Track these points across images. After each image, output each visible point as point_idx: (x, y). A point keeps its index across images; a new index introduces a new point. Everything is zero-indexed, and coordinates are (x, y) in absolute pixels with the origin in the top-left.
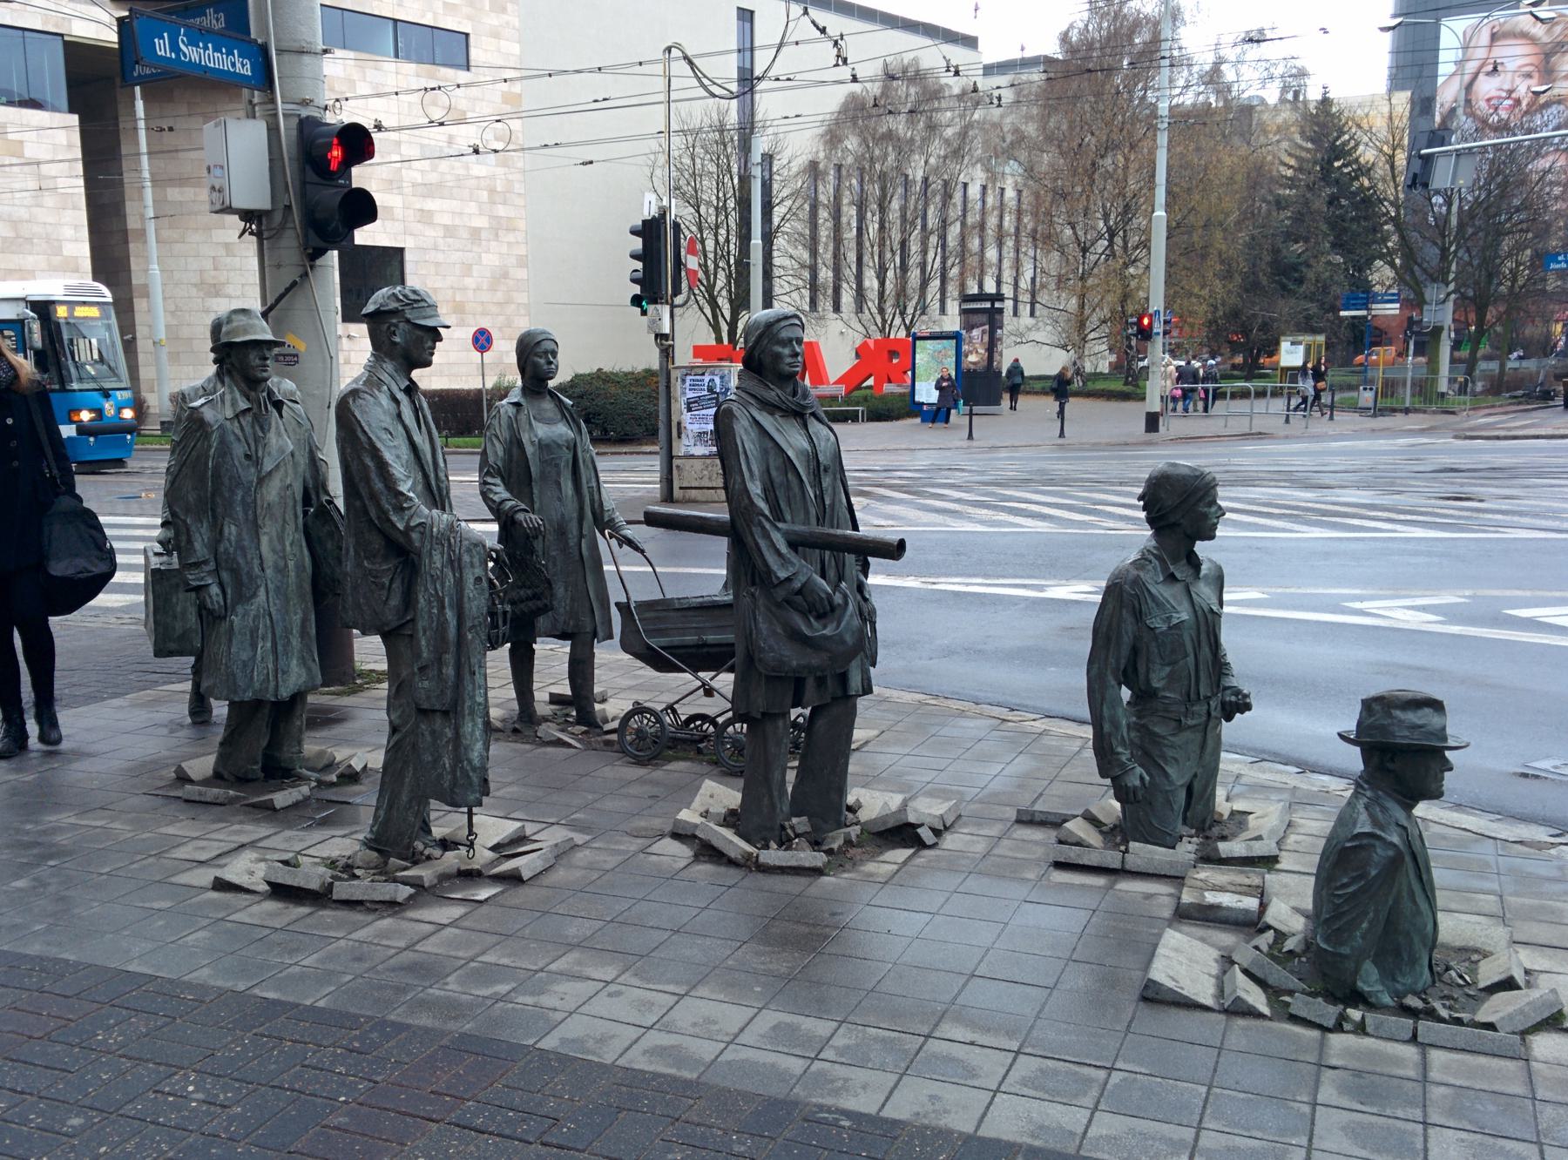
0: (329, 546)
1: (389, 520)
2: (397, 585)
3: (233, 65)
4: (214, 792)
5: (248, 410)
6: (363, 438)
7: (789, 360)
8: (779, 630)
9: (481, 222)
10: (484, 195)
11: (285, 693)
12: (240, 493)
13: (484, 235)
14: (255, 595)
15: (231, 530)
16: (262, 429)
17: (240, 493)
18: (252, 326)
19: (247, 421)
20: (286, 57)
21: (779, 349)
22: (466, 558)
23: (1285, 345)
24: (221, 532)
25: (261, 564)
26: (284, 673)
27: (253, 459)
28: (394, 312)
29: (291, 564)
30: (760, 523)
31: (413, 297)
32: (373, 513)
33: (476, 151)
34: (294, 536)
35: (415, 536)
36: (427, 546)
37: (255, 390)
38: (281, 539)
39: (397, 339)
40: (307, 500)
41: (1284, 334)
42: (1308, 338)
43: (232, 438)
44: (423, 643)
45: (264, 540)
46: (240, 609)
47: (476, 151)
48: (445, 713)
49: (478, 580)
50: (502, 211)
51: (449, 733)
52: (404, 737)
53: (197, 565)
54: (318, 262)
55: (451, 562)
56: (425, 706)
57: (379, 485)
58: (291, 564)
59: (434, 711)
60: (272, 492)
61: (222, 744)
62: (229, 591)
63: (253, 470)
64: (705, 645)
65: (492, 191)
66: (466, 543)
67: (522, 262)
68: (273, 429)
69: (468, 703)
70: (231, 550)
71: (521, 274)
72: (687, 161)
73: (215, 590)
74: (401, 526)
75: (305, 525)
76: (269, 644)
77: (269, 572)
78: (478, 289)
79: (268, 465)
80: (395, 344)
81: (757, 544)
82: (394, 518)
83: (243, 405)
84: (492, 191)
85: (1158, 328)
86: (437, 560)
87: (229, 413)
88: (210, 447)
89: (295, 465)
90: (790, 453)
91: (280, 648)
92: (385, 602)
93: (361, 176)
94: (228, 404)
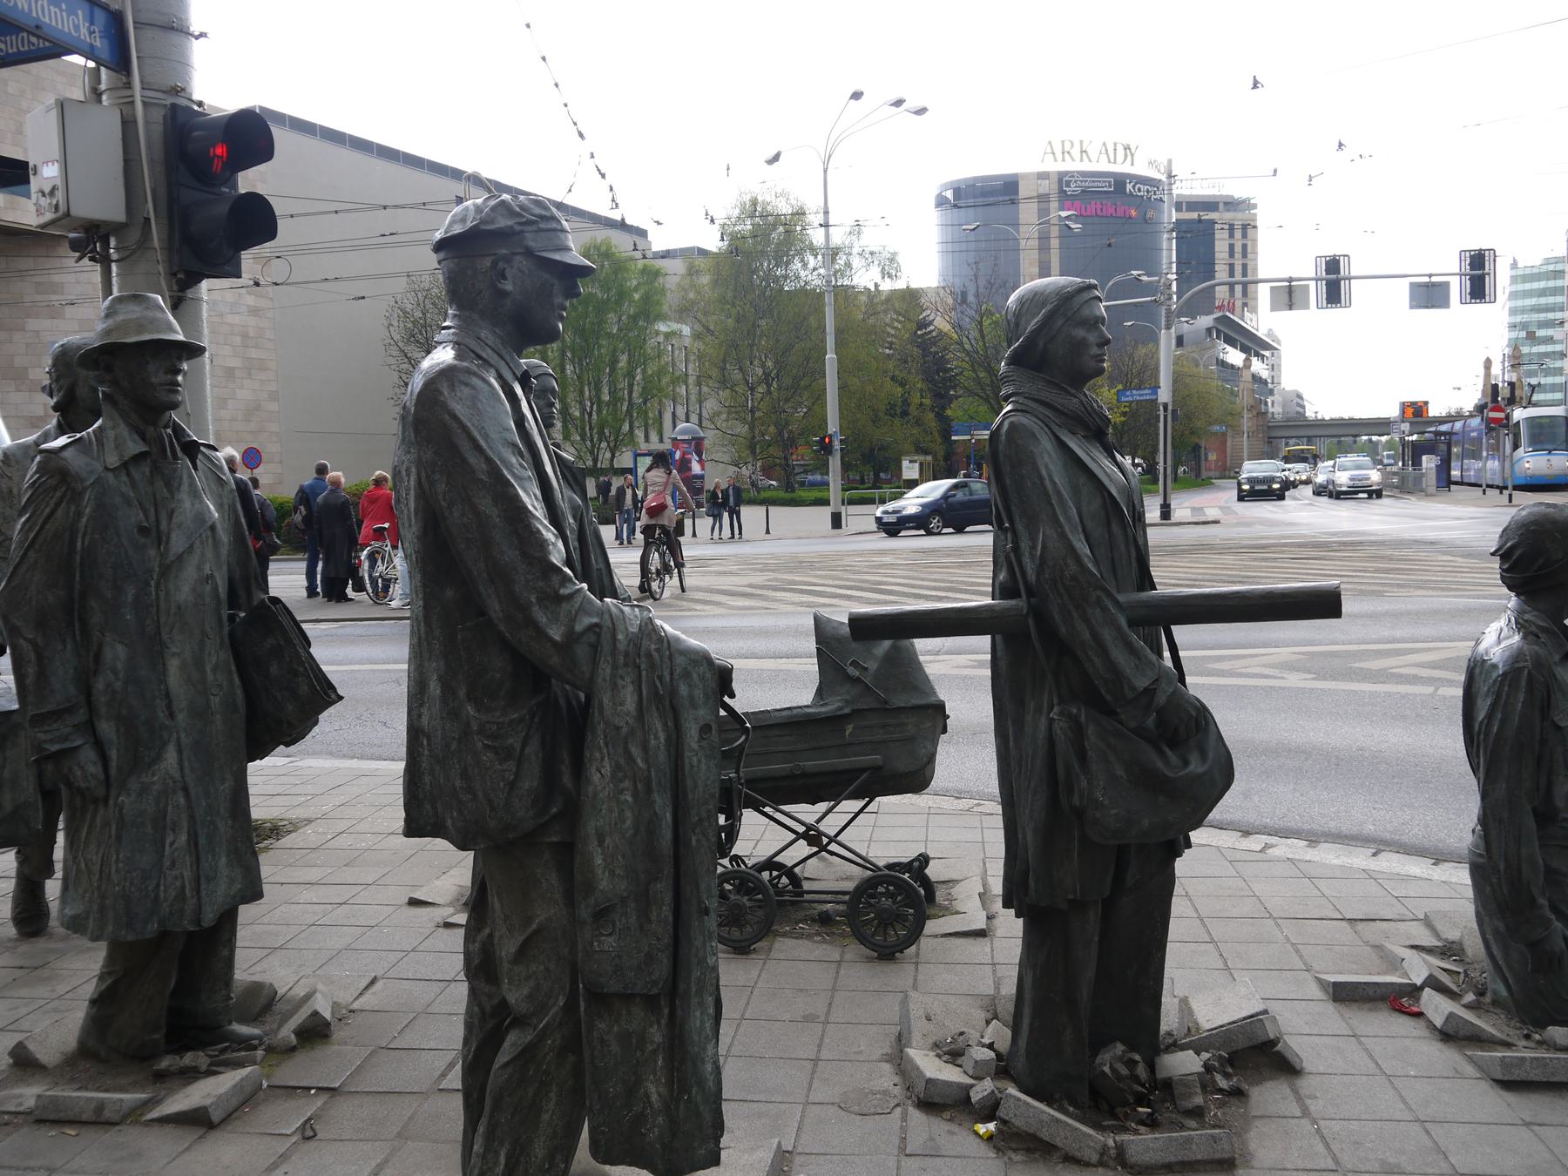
0: (274, 669)
1: (531, 623)
2: (533, 749)
3: (77, 28)
4: (84, 1097)
5: (142, 456)
6: (473, 459)
7: (1095, 350)
8: (1120, 772)
9: (234, 363)
10: (238, 340)
11: (209, 918)
12: (130, 593)
13: (238, 373)
14: (159, 758)
15: (116, 653)
16: (168, 485)
17: (130, 593)
18: (153, 321)
19: (142, 472)
20: (149, 33)
21: (1080, 333)
22: (683, 690)
23: (905, 463)
24: (98, 658)
25: (169, 706)
26: (208, 880)
27: (154, 534)
28: (503, 235)
29: (215, 701)
30: (1099, 602)
31: (538, 211)
32: (495, 608)
33: (257, 284)
34: (217, 655)
35: (581, 652)
36: (605, 669)
37: (154, 424)
38: (199, 663)
39: (508, 286)
40: (233, 600)
41: (907, 453)
42: (921, 458)
43: (118, 500)
44: (599, 861)
45: (173, 665)
46: (133, 784)
47: (257, 284)
48: (651, 1002)
49: (705, 729)
50: (254, 353)
51: (656, 1035)
52: (542, 1036)
53: (57, 715)
54: (190, 294)
55: (657, 698)
56: (613, 986)
57: (509, 554)
58: (215, 701)
59: (628, 998)
60: (184, 588)
61: (93, 1002)
62: (113, 754)
63: (152, 552)
64: (805, 775)
65: (245, 336)
66: (680, 660)
67: (273, 397)
68: (185, 487)
69: (696, 973)
70: (118, 685)
71: (274, 406)
72: (418, 314)
73: (88, 755)
74: (556, 633)
75: (232, 635)
76: (183, 838)
77: (180, 717)
78: (233, 419)
79: (177, 543)
80: (503, 294)
81: (1096, 637)
82: (541, 617)
83: (134, 447)
84: (245, 336)
85: (837, 445)
86: (621, 702)
87: (113, 460)
88: (79, 514)
89: (216, 543)
90: (1114, 492)
91: (202, 841)
92: (512, 785)
93: (249, 180)
94: (110, 445)
